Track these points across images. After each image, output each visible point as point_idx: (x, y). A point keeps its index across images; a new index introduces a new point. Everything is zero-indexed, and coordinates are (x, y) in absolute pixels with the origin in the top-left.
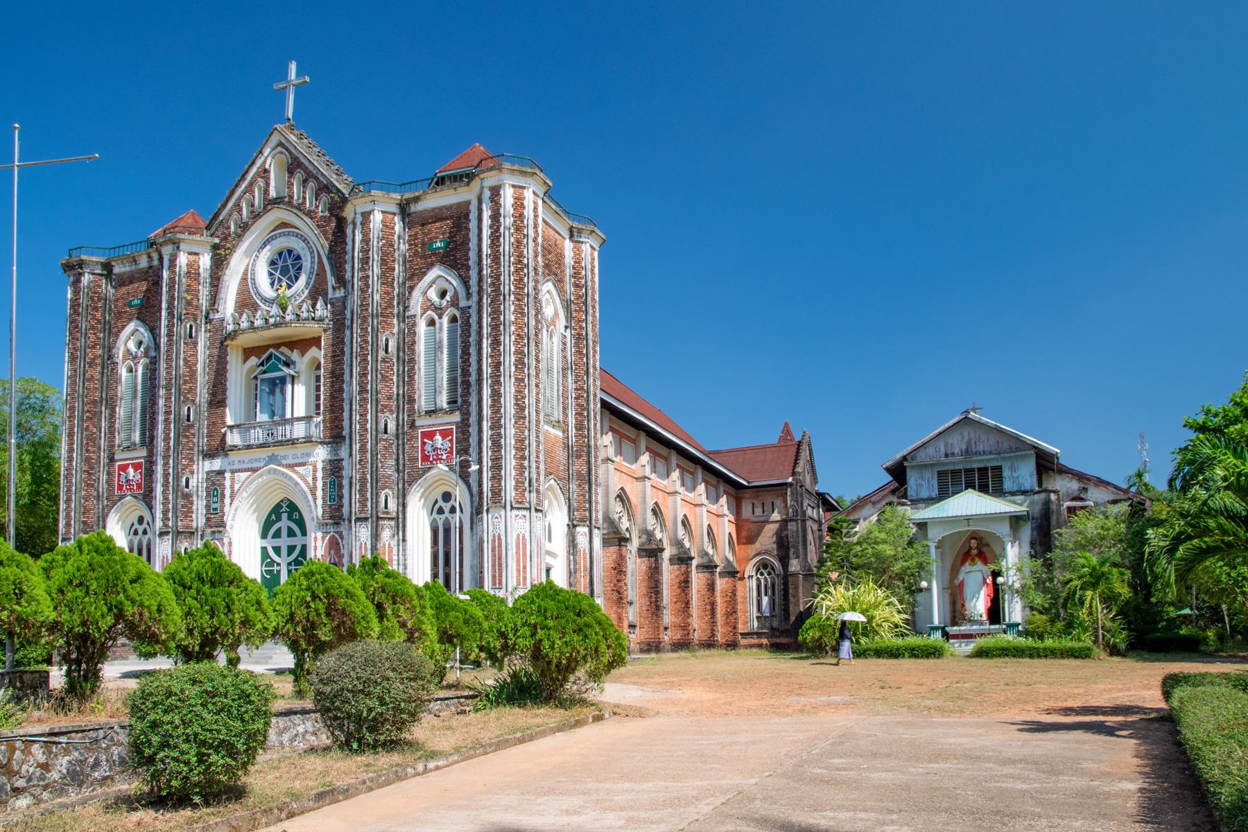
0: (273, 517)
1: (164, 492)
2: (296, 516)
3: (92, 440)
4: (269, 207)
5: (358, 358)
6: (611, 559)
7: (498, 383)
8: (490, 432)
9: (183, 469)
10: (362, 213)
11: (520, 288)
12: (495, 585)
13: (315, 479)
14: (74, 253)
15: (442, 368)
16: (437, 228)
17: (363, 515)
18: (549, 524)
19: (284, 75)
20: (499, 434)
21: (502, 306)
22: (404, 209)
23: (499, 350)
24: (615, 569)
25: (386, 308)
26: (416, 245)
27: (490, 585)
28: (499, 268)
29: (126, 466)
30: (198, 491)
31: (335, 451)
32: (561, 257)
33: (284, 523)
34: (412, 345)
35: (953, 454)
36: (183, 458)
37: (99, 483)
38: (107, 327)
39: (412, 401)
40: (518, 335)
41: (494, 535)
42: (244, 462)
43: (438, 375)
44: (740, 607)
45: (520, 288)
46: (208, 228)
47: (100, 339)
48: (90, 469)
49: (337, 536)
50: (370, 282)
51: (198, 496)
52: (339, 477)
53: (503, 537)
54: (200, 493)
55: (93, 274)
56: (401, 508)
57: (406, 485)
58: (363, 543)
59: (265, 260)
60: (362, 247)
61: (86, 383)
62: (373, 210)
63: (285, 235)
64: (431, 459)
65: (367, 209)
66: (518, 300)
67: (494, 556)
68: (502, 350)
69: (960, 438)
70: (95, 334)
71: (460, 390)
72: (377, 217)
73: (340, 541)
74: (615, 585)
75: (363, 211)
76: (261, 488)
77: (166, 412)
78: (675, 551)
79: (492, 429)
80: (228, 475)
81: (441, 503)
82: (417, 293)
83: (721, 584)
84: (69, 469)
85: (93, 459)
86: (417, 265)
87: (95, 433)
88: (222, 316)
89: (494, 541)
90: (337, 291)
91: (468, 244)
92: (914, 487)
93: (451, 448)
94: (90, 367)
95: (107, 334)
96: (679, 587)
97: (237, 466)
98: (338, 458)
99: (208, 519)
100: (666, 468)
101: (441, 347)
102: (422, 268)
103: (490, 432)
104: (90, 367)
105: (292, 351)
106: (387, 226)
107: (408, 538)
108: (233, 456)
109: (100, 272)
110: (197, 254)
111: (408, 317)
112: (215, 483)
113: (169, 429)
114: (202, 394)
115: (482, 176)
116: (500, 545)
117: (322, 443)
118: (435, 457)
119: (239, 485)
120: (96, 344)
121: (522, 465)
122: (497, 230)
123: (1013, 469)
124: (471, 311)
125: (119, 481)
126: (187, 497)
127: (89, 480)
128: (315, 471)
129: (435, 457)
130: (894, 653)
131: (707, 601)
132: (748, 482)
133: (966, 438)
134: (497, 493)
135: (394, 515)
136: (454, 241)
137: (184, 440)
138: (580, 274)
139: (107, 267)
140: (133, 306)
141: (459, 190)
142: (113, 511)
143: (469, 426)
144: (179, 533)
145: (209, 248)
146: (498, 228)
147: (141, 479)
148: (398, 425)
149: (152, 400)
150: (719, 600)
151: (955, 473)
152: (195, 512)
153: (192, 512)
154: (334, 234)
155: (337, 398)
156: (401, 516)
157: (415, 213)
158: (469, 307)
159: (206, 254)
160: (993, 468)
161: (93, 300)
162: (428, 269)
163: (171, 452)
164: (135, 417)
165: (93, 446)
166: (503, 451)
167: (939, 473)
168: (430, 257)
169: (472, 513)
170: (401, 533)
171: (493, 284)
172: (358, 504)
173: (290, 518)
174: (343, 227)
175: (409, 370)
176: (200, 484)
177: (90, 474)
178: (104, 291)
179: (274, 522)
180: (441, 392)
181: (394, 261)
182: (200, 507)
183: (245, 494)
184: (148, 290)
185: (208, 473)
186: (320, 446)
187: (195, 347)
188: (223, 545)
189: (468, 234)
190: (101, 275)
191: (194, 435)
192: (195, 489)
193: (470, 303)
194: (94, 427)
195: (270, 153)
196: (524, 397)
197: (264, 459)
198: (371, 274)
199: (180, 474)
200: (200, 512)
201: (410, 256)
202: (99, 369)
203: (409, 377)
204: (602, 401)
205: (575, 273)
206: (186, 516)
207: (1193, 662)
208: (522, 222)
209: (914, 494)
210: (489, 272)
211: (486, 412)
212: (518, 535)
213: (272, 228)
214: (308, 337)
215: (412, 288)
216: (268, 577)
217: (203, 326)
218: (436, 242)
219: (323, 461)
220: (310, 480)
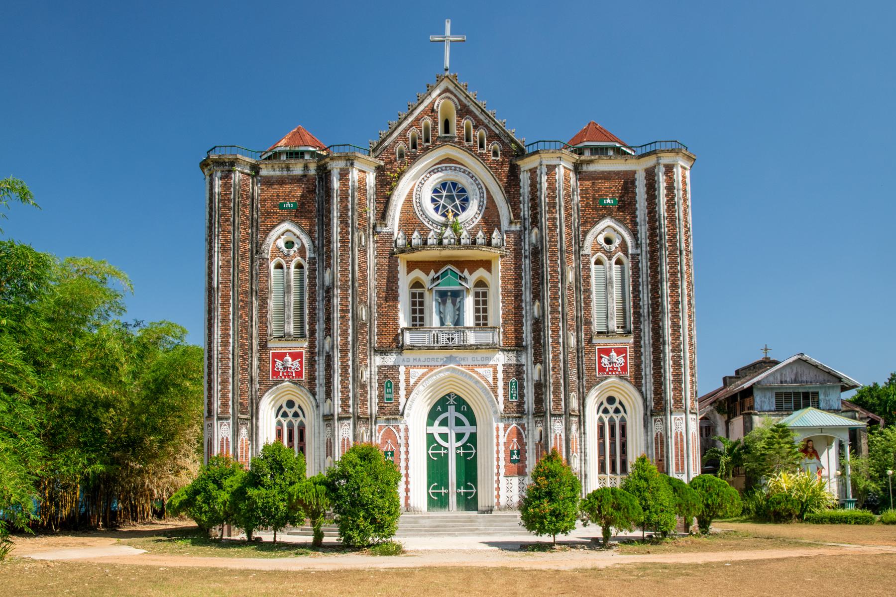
0: (439, 408)
1: (342, 382)
3: (246, 327)
5: (549, 284)
8: (671, 354)
9: (360, 363)
13: (495, 379)
16: (607, 188)
17: (557, 412)
20: (679, 356)
21: (679, 259)
23: (677, 292)
27: (674, 471)
28: (675, 229)
29: (284, 354)
30: (371, 382)
31: (518, 357)
33: (451, 413)
34: (587, 278)
35: (786, 382)
36: (360, 353)
37: (252, 368)
38: (255, 224)
39: (588, 323)
41: (677, 433)
42: (419, 360)
46: (374, 151)
48: (246, 353)
49: (519, 427)
50: (558, 223)
51: (371, 387)
52: (520, 379)
53: (684, 435)
54: (373, 384)
56: (582, 407)
57: (585, 389)
58: (558, 435)
60: (549, 194)
61: (240, 274)
62: (558, 165)
63: (451, 169)
64: (607, 370)
67: (677, 448)
68: (680, 292)
69: (790, 371)
70: (245, 229)
73: (522, 431)
75: (549, 164)
77: (342, 310)
79: (672, 351)
80: (402, 369)
82: (590, 238)
84: (224, 353)
86: (590, 214)
87: (247, 322)
88: (390, 230)
90: (513, 225)
91: (635, 205)
92: (759, 403)
93: (626, 363)
94: (242, 259)
97: (411, 363)
99: (381, 408)
101: (611, 283)
102: (594, 218)
103: (671, 354)
104: (242, 259)
107: (587, 431)
108: (407, 354)
110: (364, 172)
111: (582, 255)
112: (388, 378)
113: (347, 326)
114: (373, 296)
116: (682, 440)
118: (611, 369)
119: (415, 380)
120: (246, 239)
122: (673, 199)
123: (826, 395)
126: (363, 386)
127: (244, 364)
128: (495, 372)
130: (833, 520)
133: (795, 371)
134: (678, 401)
135: (577, 413)
136: (622, 201)
137: (360, 337)
139: (255, 168)
140: (285, 208)
141: (629, 161)
142: (267, 394)
144: (359, 418)
147: (301, 367)
148: (578, 341)
149: (311, 297)
151: (788, 395)
153: (367, 401)
154: (508, 177)
157: (585, 172)
159: (371, 173)
160: (813, 393)
161: (243, 198)
162: (600, 219)
163: (350, 347)
164: (289, 310)
166: (683, 369)
167: (777, 394)
168: (602, 210)
169: (645, 414)
171: (670, 241)
172: (552, 404)
174: (516, 172)
176: (373, 376)
177: (244, 359)
179: (440, 413)
180: (612, 318)
181: (571, 208)
182: (373, 396)
184: (302, 196)
185: (379, 367)
186: (500, 352)
187: (366, 255)
190: (248, 175)
191: (366, 332)
192: (369, 381)
194: (247, 316)
195: (439, 95)
197: (442, 359)
198: (558, 216)
200: (373, 400)
202: (249, 262)
203: (585, 303)
207: (88, 536)
209: (759, 407)
211: (668, 338)
213: (437, 161)
214: (471, 259)
215: (585, 233)
216: (435, 459)
217: (371, 236)
218: (606, 199)
219: (504, 365)
220: (491, 380)
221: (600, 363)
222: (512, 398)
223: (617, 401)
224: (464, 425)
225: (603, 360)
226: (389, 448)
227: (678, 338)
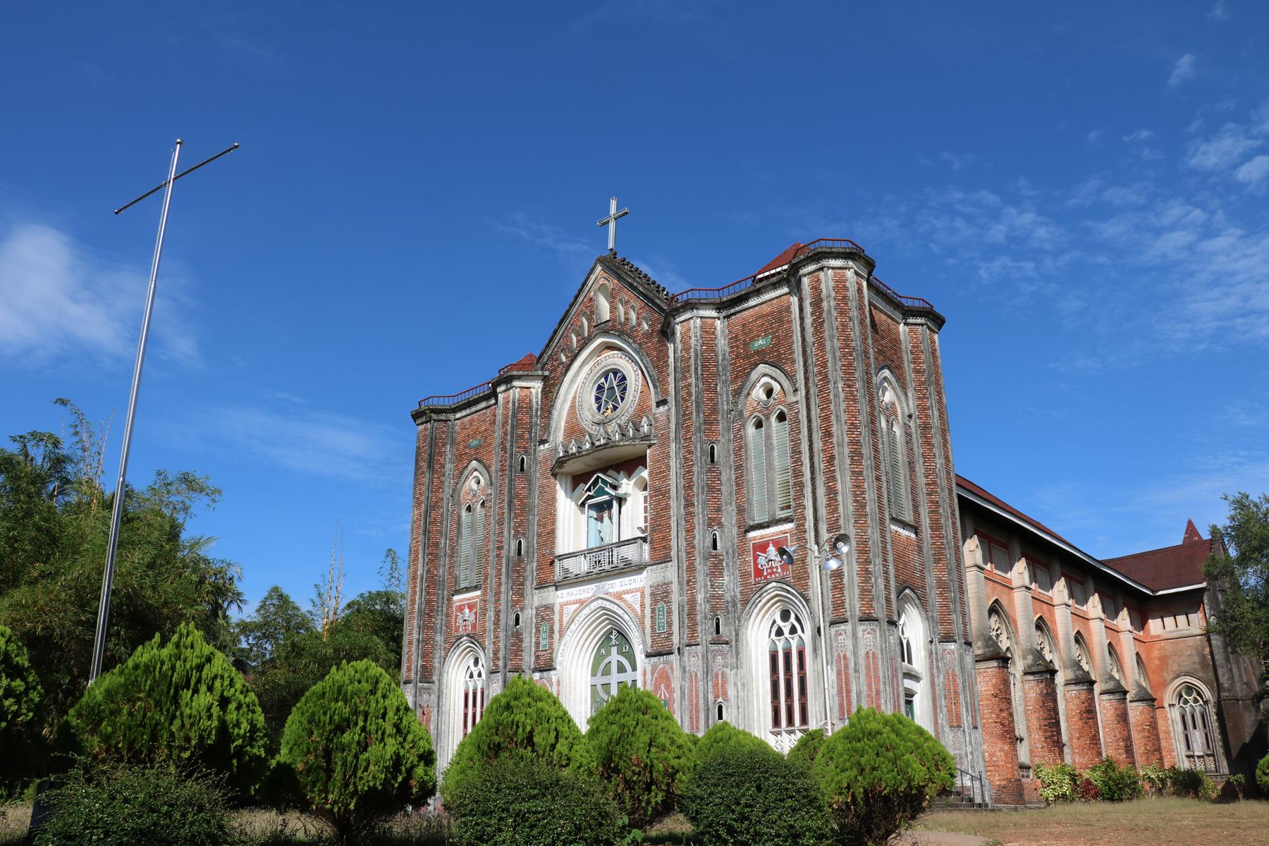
0: (603, 651)
6: (990, 684)
11: (850, 373)
14: (423, 404)
18: (908, 642)
23: (831, 443)
24: (996, 697)
25: (710, 415)
26: (738, 347)
32: (897, 342)
33: (614, 657)
40: (852, 424)
41: (839, 655)
44: (1163, 744)
45: (850, 373)
64: (765, 574)
66: (849, 386)
71: (792, 493)
74: (998, 716)
78: (1070, 675)
83: (1136, 712)
91: (791, 337)
96: (1080, 719)
100: (1048, 578)
102: (745, 369)
105: (619, 474)
118: (769, 571)
121: (867, 571)
124: (799, 406)
125: (456, 622)
128: (643, 597)
131: (1118, 736)
132: (1153, 592)
138: (919, 358)
143: (805, 532)
146: (821, 314)
147: (476, 619)
150: (1136, 736)
155: (664, 516)
158: (797, 402)
173: (620, 652)
183: (573, 627)
188: (551, 684)
189: (790, 327)
193: (798, 398)
196: (863, 493)
204: (959, 497)
205: (914, 358)
206: (516, 655)
208: (846, 304)
210: (814, 361)
212: (868, 653)
214: (634, 457)
220: (638, 609)
221: (756, 565)
222: (659, 629)
223: (793, 616)
224: (626, 671)
225: (759, 561)
226: (663, 697)
227: (836, 510)
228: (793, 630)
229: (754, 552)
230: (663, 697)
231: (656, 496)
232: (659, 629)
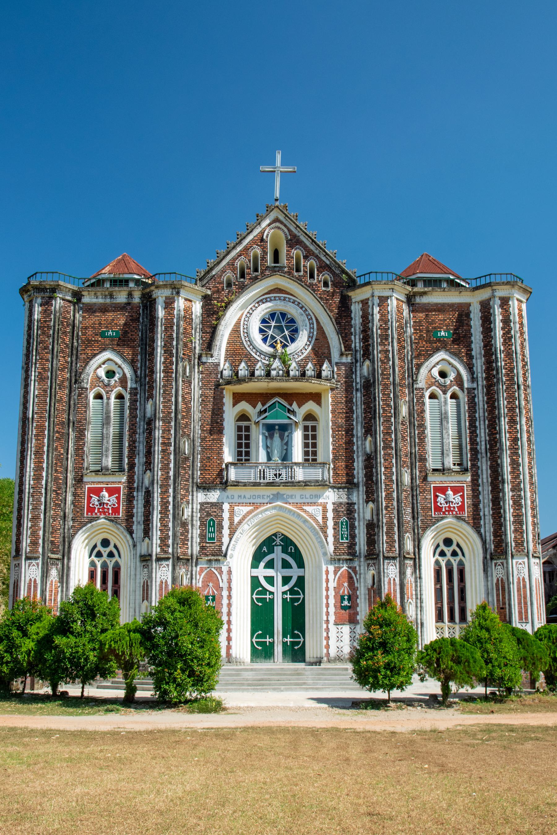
0: (265, 549)
1: (162, 519)
2: (291, 549)
3: (61, 460)
4: (267, 272)
5: (382, 419)
7: (517, 454)
8: (511, 494)
10: (379, 297)
12: (522, 619)
13: (325, 518)
15: (448, 435)
16: (441, 320)
17: (391, 555)
19: (272, 162)
21: (517, 394)
22: (410, 300)
26: (421, 331)
30: (192, 520)
31: (349, 495)
33: (278, 555)
36: (181, 488)
37: (65, 504)
38: (75, 352)
41: (519, 579)
42: (245, 497)
43: (444, 440)
46: (201, 280)
47: (68, 363)
52: (351, 518)
53: (527, 580)
55: (63, 300)
57: (420, 530)
58: (392, 579)
59: (259, 318)
60: (381, 325)
61: (57, 404)
62: (391, 296)
63: (280, 299)
64: (444, 510)
65: (385, 294)
68: (518, 428)
70: (64, 357)
72: (393, 304)
73: (353, 575)
75: (381, 295)
76: (265, 520)
79: (512, 490)
80: (226, 507)
81: (99, 548)
82: (424, 371)
84: (36, 487)
85: (60, 479)
86: (423, 347)
87: (62, 454)
88: (216, 361)
89: (519, 583)
91: (470, 337)
95: (74, 359)
97: (236, 500)
98: (350, 502)
99: (202, 548)
103: (511, 494)
106: (400, 311)
107: (423, 576)
108: (231, 491)
109: (69, 298)
110: (191, 301)
111: (416, 389)
113: (168, 460)
115: (494, 288)
116: (525, 586)
117: (333, 487)
118: (447, 509)
120: (65, 368)
122: (509, 332)
126: (184, 524)
127: (57, 500)
128: (325, 510)
129: (447, 509)
134: (519, 543)
135: (412, 556)
137: (182, 472)
139: (77, 295)
140: (108, 337)
142: (80, 532)
145: (201, 297)
148: (412, 479)
152: (190, 540)
154: (339, 308)
156: (417, 557)
157: (418, 304)
159: (198, 302)
161: (63, 325)
162: (434, 352)
164: (108, 442)
165: (61, 467)
166: (523, 510)
169: (485, 558)
170: (418, 571)
172: (385, 545)
173: (284, 551)
175: (419, 433)
178: (72, 318)
179: (265, 555)
180: (448, 455)
181: (404, 341)
182: (194, 535)
184: (125, 324)
185: (202, 504)
186: (330, 490)
187: (190, 386)
189: (470, 330)
192: (190, 518)
197: (268, 496)
198: (390, 348)
199: (180, 503)
200: (194, 540)
201: (415, 339)
202: (67, 391)
203: (419, 439)
206: (184, 544)
214: (304, 392)
215: (419, 367)
216: (260, 604)
217: (196, 367)
218: (441, 331)
220: (320, 519)
221: (436, 502)
225: (439, 499)
226: (211, 592)
228: (454, 554)
229: (434, 493)
230: (211, 592)
231: (339, 431)
232: (342, 539)
